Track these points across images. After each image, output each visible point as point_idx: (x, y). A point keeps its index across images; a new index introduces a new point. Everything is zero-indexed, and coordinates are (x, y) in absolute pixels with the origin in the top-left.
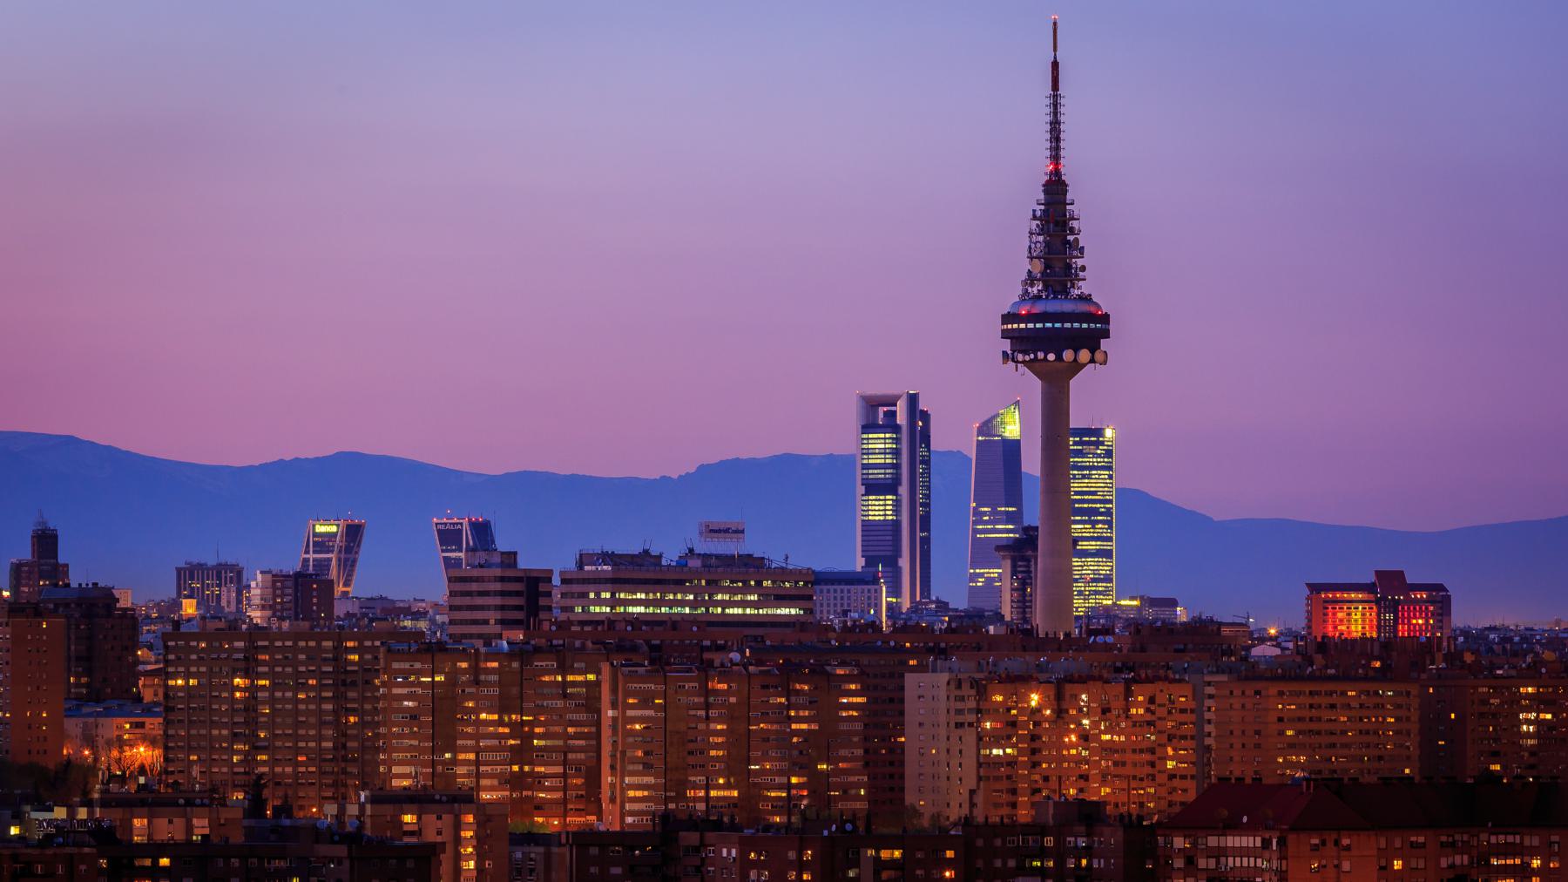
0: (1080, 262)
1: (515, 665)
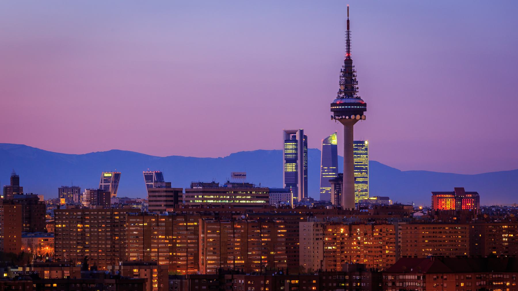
0: (357, 86)
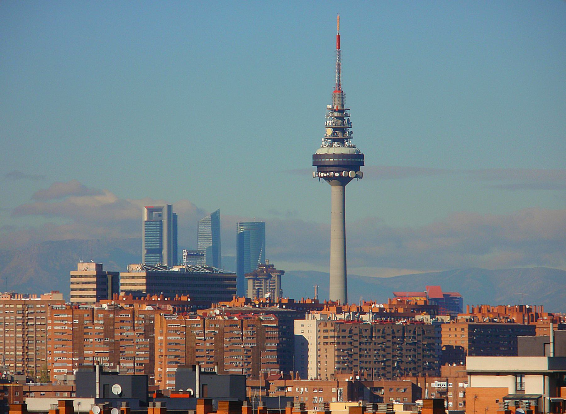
0: (350, 130)
1: (111, 315)
